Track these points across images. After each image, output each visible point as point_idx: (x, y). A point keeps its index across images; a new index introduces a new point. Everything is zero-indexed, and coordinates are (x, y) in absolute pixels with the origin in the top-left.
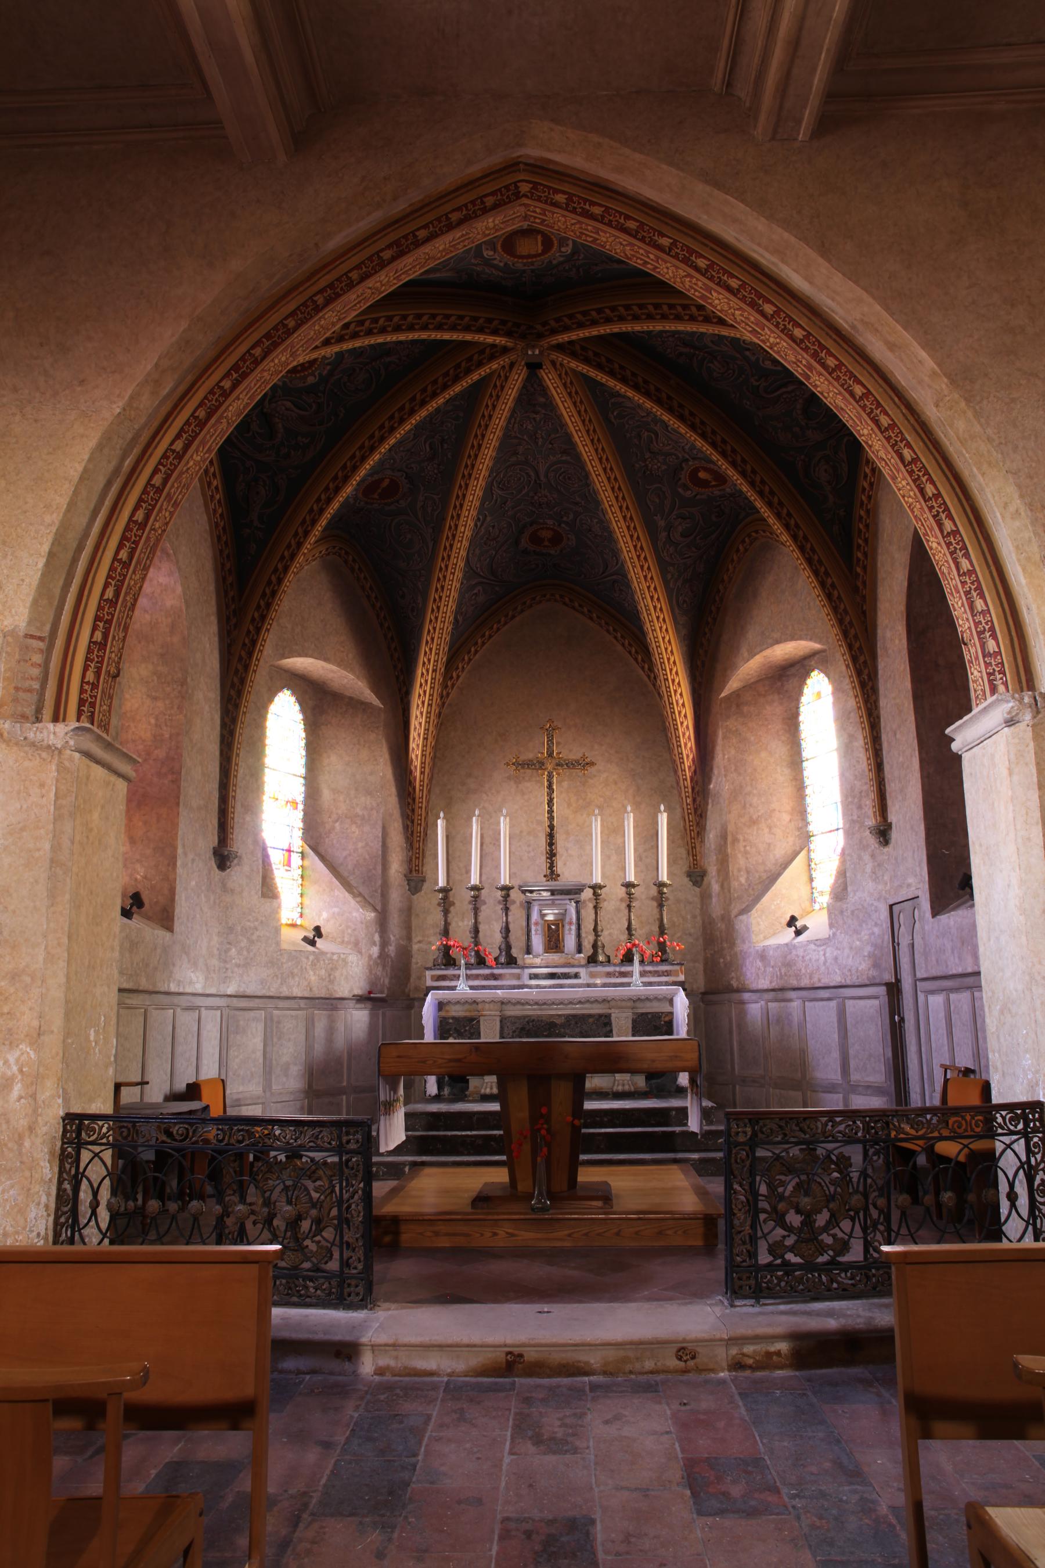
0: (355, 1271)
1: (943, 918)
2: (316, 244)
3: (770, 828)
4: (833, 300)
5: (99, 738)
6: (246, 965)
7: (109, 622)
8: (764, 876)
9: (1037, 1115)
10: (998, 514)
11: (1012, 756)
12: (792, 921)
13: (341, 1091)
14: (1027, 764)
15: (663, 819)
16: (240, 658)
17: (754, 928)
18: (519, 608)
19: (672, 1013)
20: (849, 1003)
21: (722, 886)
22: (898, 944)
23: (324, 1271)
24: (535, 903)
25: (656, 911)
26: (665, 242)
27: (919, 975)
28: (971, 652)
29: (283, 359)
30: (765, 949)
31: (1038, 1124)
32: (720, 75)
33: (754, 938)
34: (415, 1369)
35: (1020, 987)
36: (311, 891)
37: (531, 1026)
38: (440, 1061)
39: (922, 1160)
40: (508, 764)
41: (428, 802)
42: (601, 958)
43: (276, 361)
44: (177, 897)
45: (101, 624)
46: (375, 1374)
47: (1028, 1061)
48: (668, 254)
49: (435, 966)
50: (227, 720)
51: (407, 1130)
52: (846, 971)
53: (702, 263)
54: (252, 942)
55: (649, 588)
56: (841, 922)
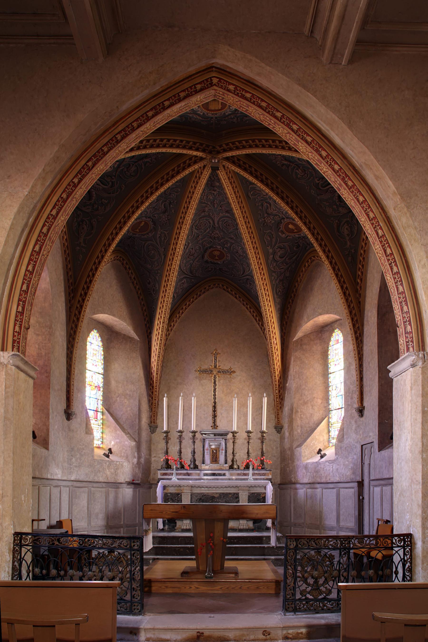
0: (137, 600)
1: (383, 452)
2: (117, 107)
3: (312, 406)
4: (353, 151)
5: (22, 359)
6: (79, 466)
7: (24, 302)
8: (309, 429)
9: (409, 539)
10: (416, 265)
11: (413, 381)
12: (320, 451)
13: (121, 527)
14: (418, 385)
15: (265, 400)
16: (75, 315)
17: (303, 454)
18: (203, 291)
19: (265, 493)
20: (342, 490)
21: (290, 434)
22: (364, 464)
23: (124, 600)
24: (207, 440)
25: (260, 445)
26: (279, 115)
27: (371, 478)
28: (400, 331)
29: (102, 168)
30: (307, 464)
31: (409, 543)
32: (308, 27)
33: (302, 459)
34: (161, 639)
35: (407, 485)
36: (106, 431)
37: (204, 498)
38: (169, 512)
39: (365, 560)
40: (196, 371)
41: (159, 388)
42: (235, 467)
43: (98, 169)
44: (50, 434)
45: (21, 303)
46: (146, 640)
47: (408, 517)
48: (280, 121)
49: (162, 468)
50: (69, 346)
51: (153, 544)
52: (341, 475)
53: (295, 127)
54: (82, 455)
55: (263, 284)
56: (340, 453)
